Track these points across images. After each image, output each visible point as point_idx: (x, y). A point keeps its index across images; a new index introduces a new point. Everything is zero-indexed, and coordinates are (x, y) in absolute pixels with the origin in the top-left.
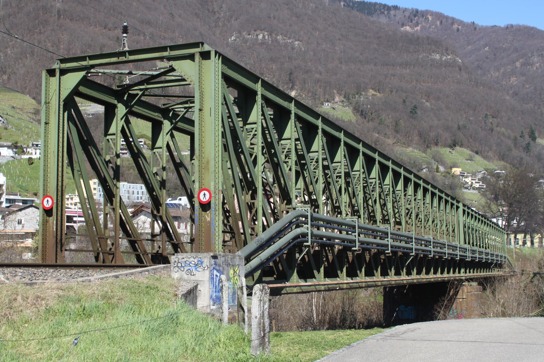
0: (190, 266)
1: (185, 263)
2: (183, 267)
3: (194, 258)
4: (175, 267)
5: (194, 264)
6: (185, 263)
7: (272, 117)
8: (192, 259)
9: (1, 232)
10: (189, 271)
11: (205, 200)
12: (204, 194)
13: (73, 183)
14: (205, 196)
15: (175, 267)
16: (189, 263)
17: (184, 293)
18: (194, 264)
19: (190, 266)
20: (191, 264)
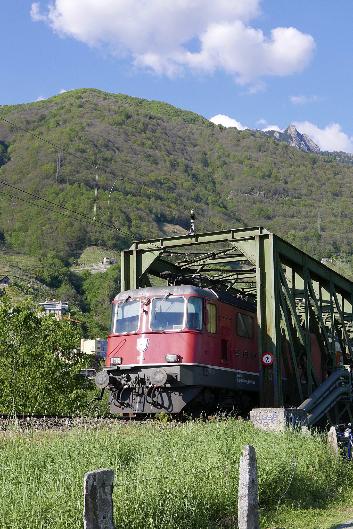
0: (267, 419)
1: (263, 417)
2: (261, 420)
3: (271, 413)
4: (254, 420)
5: (271, 418)
6: (263, 417)
7: (296, 308)
8: (269, 413)
9: (82, 526)
10: (266, 423)
11: (267, 363)
12: (267, 357)
13: (302, 247)
14: (267, 359)
15: (254, 420)
16: (266, 417)
17: (108, 382)
18: (271, 418)
19: (267, 419)
20: (267, 418)
